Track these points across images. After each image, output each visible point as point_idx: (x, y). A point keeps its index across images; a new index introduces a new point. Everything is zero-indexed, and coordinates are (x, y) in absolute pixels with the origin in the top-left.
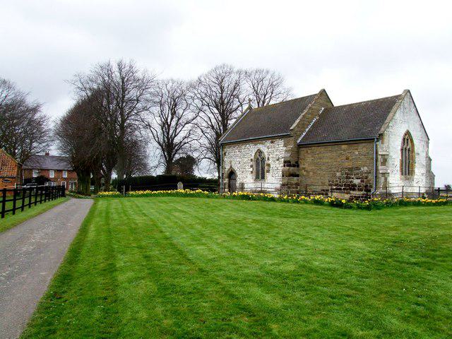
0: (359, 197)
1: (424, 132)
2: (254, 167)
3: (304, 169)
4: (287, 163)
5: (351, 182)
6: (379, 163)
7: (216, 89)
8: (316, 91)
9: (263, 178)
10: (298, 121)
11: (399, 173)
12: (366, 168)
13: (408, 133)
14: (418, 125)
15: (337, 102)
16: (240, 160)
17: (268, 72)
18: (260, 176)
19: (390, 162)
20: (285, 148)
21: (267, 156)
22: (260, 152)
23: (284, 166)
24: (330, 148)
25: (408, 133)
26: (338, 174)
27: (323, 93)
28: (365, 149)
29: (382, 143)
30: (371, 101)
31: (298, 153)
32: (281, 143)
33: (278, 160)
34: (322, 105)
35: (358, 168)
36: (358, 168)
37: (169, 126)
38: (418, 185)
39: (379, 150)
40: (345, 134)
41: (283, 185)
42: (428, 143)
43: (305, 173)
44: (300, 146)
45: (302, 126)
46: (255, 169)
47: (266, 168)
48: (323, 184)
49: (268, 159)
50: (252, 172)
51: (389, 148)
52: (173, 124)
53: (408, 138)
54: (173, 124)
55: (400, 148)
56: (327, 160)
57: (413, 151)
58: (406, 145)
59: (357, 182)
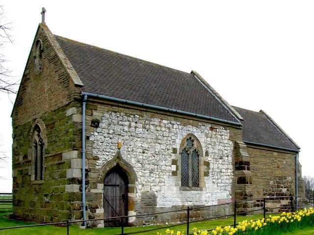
2: (179, 164)
9: (197, 184)
16: (146, 146)
22: (191, 139)
24: (264, 153)
26: (271, 182)
33: (221, 158)
47: (203, 168)
56: (262, 166)
59: (284, 190)
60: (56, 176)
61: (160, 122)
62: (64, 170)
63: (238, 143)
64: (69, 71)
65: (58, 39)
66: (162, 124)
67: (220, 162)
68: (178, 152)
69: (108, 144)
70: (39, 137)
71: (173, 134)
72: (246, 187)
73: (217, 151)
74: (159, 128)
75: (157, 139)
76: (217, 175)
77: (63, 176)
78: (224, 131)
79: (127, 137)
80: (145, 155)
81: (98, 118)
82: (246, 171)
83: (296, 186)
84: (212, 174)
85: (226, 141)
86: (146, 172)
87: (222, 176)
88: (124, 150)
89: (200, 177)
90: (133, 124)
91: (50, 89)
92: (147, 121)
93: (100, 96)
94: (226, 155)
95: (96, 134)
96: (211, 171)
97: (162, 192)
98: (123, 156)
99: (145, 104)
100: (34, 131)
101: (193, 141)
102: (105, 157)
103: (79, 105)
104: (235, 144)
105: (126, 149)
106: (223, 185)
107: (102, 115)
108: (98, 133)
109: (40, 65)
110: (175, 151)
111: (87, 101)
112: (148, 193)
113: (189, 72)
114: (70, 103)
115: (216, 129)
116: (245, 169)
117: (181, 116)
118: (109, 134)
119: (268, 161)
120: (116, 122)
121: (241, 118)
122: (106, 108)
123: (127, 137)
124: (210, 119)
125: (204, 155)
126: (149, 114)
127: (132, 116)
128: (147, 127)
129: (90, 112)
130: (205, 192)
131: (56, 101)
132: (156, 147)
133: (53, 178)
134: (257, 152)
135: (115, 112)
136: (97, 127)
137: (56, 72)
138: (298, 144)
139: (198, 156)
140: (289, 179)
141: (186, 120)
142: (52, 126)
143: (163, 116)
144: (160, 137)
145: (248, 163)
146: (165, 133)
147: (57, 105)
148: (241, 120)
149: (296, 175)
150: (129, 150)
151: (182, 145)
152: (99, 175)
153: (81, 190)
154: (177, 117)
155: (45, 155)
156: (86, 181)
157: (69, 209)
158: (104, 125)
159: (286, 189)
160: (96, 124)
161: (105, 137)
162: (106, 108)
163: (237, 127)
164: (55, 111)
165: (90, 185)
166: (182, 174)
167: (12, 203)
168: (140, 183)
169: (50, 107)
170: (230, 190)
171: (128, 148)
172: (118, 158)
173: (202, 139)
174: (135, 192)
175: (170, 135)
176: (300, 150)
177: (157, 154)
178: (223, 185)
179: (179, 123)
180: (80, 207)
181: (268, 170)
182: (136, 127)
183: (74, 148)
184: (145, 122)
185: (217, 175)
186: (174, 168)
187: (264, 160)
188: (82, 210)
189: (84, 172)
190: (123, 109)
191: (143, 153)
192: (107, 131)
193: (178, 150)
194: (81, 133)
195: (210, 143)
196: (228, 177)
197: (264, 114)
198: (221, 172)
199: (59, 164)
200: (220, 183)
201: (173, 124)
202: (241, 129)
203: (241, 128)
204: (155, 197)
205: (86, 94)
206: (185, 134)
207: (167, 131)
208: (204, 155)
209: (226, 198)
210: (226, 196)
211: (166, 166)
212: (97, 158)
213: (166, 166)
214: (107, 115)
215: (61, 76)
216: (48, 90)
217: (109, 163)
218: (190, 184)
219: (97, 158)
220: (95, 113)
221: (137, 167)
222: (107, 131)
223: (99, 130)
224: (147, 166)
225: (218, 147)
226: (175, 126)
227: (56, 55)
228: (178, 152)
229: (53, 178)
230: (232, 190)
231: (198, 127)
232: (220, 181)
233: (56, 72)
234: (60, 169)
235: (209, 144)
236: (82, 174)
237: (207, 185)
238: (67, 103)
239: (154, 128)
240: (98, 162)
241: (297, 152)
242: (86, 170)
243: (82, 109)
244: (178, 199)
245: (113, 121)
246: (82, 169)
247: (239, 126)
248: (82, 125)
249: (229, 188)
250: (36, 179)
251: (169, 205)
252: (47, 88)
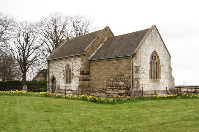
0: (123, 94)
1: (167, 52)
3: (93, 76)
4: (82, 72)
5: (119, 84)
6: (134, 72)
7: (52, 28)
8: (102, 27)
9: (70, 82)
10: (89, 46)
11: (149, 78)
12: (127, 75)
13: (155, 52)
14: (162, 47)
15: (116, 34)
17: (83, 17)
18: (68, 81)
19: (141, 71)
20: (81, 63)
21: (72, 68)
22: (68, 66)
23: (80, 74)
24: (107, 63)
25: (155, 52)
26: (112, 79)
27: (107, 29)
28: (126, 63)
29: (136, 59)
30: (134, 33)
31: (89, 66)
32: (79, 59)
34: (106, 36)
35: (122, 75)
36: (122, 75)
37: (25, 50)
38: (163, 85)
39: (134, 63)
40: (115, 54)
41: (79, 87)
42: (170, 59)
43: (93, 78)
44: (90, 61)
45: (92, 49)
46: (66, 76)
47: (71, 75)
48: (103, 85)
49: (73, 70)
50: (64, 78)
51: (140, 61)
52: (27, 48)
53: (155, 56)
54: (27, 48)
55: (149, 62)
57: (159, 63)
58: (154, 60)
59: (122, 84)
119: (109, 66)
186: (64, 76)
226: (64, 62)
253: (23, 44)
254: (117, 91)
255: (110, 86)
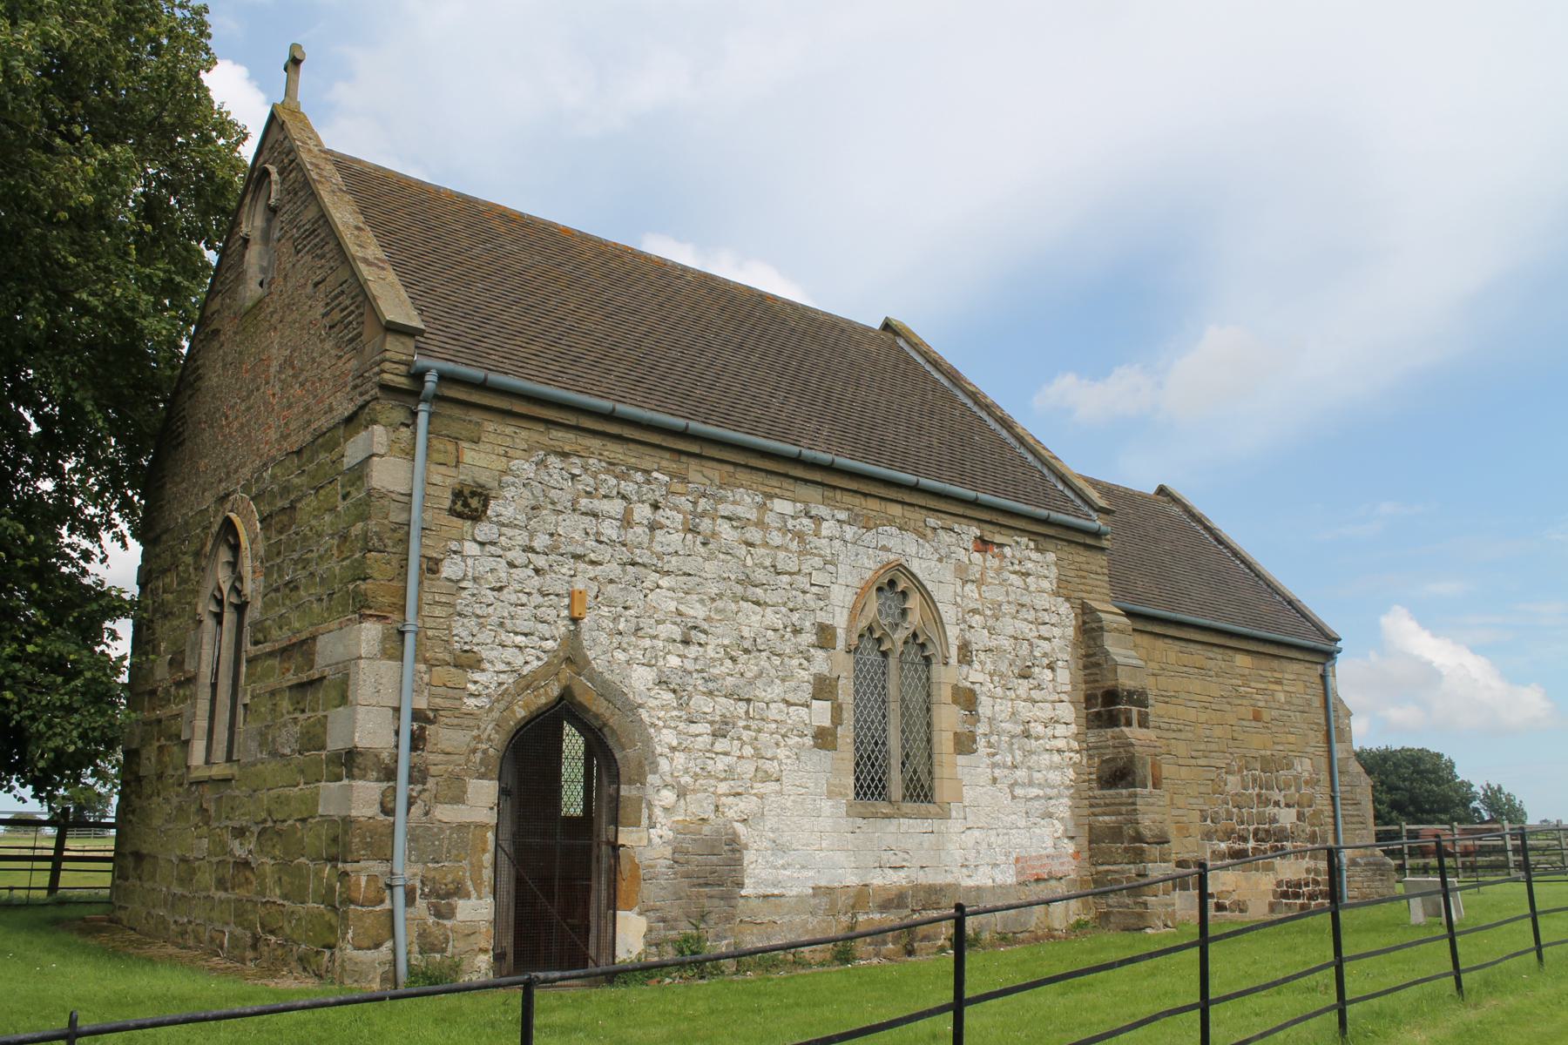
9: (921, 791)
16: (697, 612)
24: (1198, 655)
47: (948, 718)
56: (1192, 714)
59: (1287, 818)
60: (287, 740)
61: (762, 507)
62: (320, 714)
63: (1093, 611)
64: (366, 271)
65: (344, 164)
66: (769, 518)
67: (1022, 692)
68: (840, 644)
69: (524, 599)
70: (233, 572)
71: (818, 562)
72: (1139, 801)
73: (1007, 644)
74: (754, 535)
75: (747, 581)
76: (1011, 751)
77: (313, 740)
78: (1035, 555)
79: (613, 569)
80: (693, 651)
81: (484, 478)
82: (1134, 733)
83: (1333, 798)
84: (990, 745)
85: (1043, 601)
86: (694, 729)
87: (1031, 752)
88: (600, 628)
89: (936, 758)
90: (642, 512)
91: (288, 362)
92: (702, 501)
93: (494, 377)
94: (1046, 661)
95: (471, 548)
96: (982, 729)
97: (771, 822)
98: (591, 654)
99: (695, 426)
100: (215, 546)
101: (904, 594)
102: (509, 654)
103: (399, 415)
104: (1084, 613)
105: (607, 624)
106: (1034, 791)
107: (501, 464)
108: (482, 544)
109: (263, 270)
110: (825, 636)
111: (438, 398)
112: (706, 829)
113: (877, 324)
114: (362, 407)
115: (1001, 545)
116: (1129, 724)
117: (854, 485)
118: (532, 550)
120: (564, 499)
121: (1103, 503)
122: (524, 434)
123: (613, 569)
124: (975, 504)
125: (953, 660)
126: (715, 472)
127: (639, 477)
128: (705, 525)
129: (451, 447)
130: (954, 825)
131: (307, 409)
132: (741, 617)
133: (274, 754)
134: (1168, 652)
135: (564, 455)
136: (476, 517)
137: (316, 285)
138: (1331, 620)
139: (928, 660)
140: (1304, 767)
141: (873, 504)
142: (285, 518)
143: (774, 481)
144: (760, 575)
145: (1139, 698)
146: (782, 554)
147: (309, 422)
148: (1101, 510)
149: (1330, 752)
150: (621, 627)
151: (855, 612)
152: (478, 739)
153: (388, 811)
154: (834, 488)
155: (249, 649)
156: (412, 768)
157: (327, 898)
158: (508, 512)
159: (1293, 811)
160: (474, 503)
161: (511, 565)
162: (525, 435)
163: (1089, 540)
164: (299, 452)
165: (431, 783)
166: (858, 744)
167: (109, 866)
168: (669, 779)
169: (285, 437)
170: (1067, 814)
171: (615, 620)
172: (569, 660)
173: (945, 591)
174: (645, 821)
175: (806, 568)
176: (1339, 644)
177: (746, 651)
178: (1034, 791)
179: (843, 515)
180: (379, 891)
181: (1218, 731)
182: (653, 527)
183: (362, 608)
184: (695, 503)
185: (1011, 751)
186: (822, 710)
187: (1196, 685)
188: (387, 905)
189: (407, 726)
190: (596, 443)
191: (686, 642)
192: (521, 538)
193: (841, 633)
194: (405, 541)
195: (978, 606)
196: (1056, 758)
197: (1175, 500)
198: (1027, 735)
199: (302, 687)
200: (1023, 785)
201: (818, 520)
202: (1102, 549)
203: (1105, 544)
204: (735, 846)
205: (433, 366)
206: (872, 565)
207: (794, 546)
208: (953, 660)
209: (1051, 851)
210: (1049, 843)
211: (788, 704)
212: (469, 661)
213: (788, 704)
214: (527, 468)
215: (336, 297)
216: (281, 369)
217: (527, 683)
218: (896, 787)
219: (469, 661)
220: (469, 455)
221: (656, 707)
222: (521, 538)
223: (484, 530)
224: (700, 703)
225: (1008, 626)
226: (828, 528)
227: (324, 218)
228: (840, 644)
229: (274, 754)
230: (1076, 817)
231: (924, 536)
232: (1021, 774)
233: (316, 285)
234: (303, 711)
235: (975, 611)
236: (397, 733)
237: (968, 794)
238: (351, 408)
239: (735, 534)
240: (477, 676)
241: (1329, 655)
242: (417, 715)
243: (414, 433)
244: (840, 857)
245: (553, 493)
246: (397, 710)
247: (1097, 534)
248: (408, 507)
249: (1063, 807)
250: (208, 762)
251: (797, 882)
252: (277, 354)
253: (499, 855)
254: (1269, 868)
255: (1228, 836)
